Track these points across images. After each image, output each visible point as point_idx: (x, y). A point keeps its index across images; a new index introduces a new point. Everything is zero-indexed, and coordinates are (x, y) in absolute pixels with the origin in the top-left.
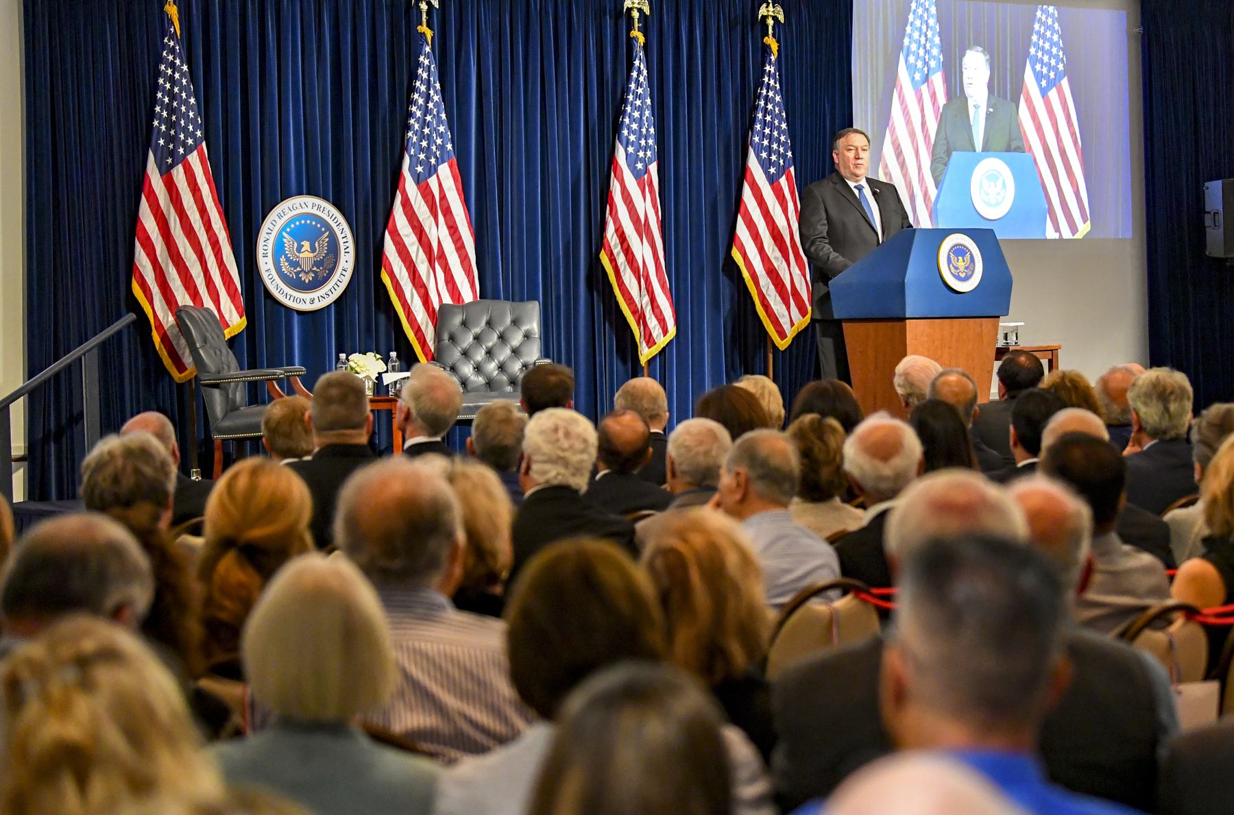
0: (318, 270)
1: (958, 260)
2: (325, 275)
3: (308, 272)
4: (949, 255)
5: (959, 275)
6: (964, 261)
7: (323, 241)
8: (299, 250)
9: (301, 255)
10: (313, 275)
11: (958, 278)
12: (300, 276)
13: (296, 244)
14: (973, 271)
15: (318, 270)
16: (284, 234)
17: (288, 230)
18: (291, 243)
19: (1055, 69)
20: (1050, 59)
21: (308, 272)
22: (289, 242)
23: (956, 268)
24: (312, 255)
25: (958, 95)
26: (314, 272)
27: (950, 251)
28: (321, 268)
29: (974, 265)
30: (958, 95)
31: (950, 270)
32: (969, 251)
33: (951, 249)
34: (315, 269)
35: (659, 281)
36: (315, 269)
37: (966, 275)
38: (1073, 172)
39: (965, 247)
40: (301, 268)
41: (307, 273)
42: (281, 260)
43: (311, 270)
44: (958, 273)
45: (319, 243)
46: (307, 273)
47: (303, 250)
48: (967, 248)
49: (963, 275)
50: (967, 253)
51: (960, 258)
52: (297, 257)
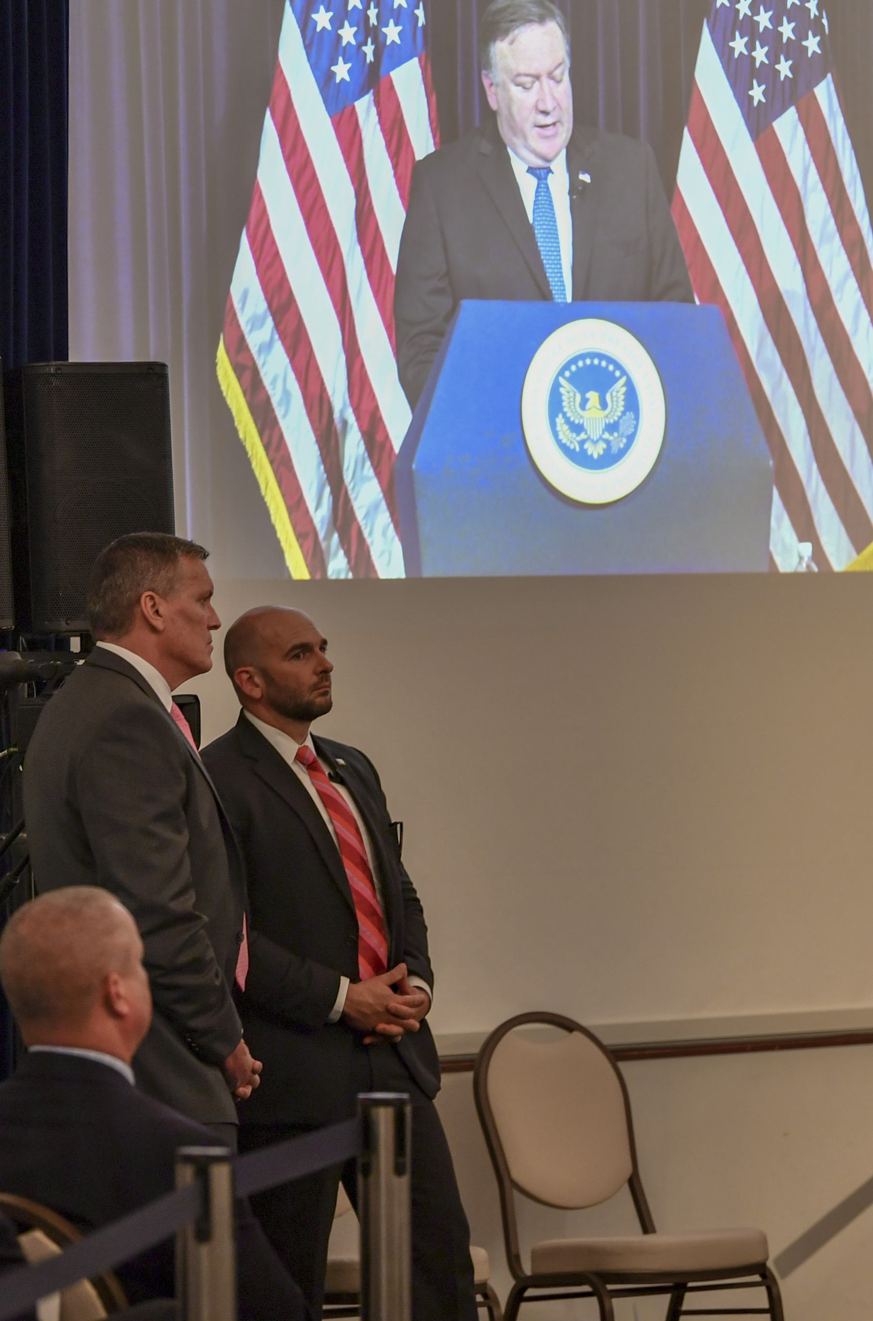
1: (584, 402)
3: (597, 441)
4: (556, 386)
5: (583, 452)
6: (604, 405)
7: (618, 392)
8: (583, 405)
11: (580, 458)
13: (578, 397)
14: (631, 438)
16: (561, 380)
17: (567, 374)
18: (572, 394)
19: (794, 50)
20: (751, 47)
21: (597, 441)
22: (568, 392)
23: (577, 428)
25: (477, 123)
26: (607, 442)
27: (561, 373)
29: (637, 418)
30: (477, 123)
31: (555, 434)
32: (624, 372)
33: (566, 367)
35: (267, 447)
37: (608, 450)
38: (517, 184)
39: (610, 360)
40: (586, 434)
41: (595, 443)
43: (601, 438)
44: (582, 443)
46: (595, 443)
47: (588, 406)
48: (618, 366)
49: (596, 451)
50: (617, 379)
51: (593, 396)
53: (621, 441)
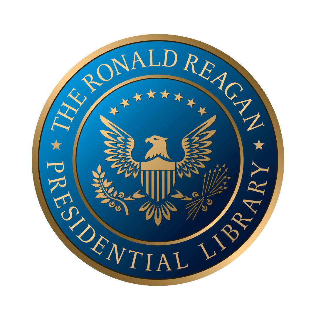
0: (187, 199)
2: (205, 209)
7: (201, 137)
9: (145, 166)
10: (175, 210)
12: (141, 210)
13: (131, 143)
15: (187, 199)
21: (162, 202)
24: (171, 166)
26: (177, 203)
28: (195, 194)
34: (179, 195)
36: (179, 195)
42: (95, 174)
45: (190, 140)
46: (158, 204)
52: (135, 169)
53: (205, 204)
